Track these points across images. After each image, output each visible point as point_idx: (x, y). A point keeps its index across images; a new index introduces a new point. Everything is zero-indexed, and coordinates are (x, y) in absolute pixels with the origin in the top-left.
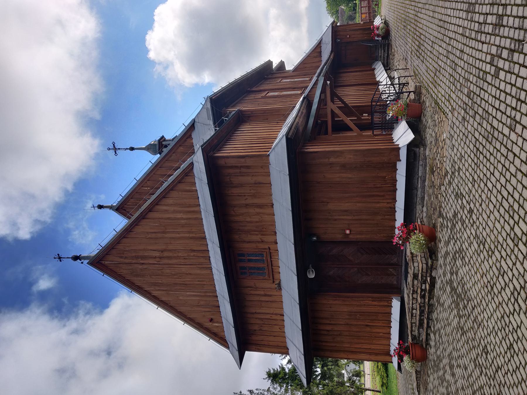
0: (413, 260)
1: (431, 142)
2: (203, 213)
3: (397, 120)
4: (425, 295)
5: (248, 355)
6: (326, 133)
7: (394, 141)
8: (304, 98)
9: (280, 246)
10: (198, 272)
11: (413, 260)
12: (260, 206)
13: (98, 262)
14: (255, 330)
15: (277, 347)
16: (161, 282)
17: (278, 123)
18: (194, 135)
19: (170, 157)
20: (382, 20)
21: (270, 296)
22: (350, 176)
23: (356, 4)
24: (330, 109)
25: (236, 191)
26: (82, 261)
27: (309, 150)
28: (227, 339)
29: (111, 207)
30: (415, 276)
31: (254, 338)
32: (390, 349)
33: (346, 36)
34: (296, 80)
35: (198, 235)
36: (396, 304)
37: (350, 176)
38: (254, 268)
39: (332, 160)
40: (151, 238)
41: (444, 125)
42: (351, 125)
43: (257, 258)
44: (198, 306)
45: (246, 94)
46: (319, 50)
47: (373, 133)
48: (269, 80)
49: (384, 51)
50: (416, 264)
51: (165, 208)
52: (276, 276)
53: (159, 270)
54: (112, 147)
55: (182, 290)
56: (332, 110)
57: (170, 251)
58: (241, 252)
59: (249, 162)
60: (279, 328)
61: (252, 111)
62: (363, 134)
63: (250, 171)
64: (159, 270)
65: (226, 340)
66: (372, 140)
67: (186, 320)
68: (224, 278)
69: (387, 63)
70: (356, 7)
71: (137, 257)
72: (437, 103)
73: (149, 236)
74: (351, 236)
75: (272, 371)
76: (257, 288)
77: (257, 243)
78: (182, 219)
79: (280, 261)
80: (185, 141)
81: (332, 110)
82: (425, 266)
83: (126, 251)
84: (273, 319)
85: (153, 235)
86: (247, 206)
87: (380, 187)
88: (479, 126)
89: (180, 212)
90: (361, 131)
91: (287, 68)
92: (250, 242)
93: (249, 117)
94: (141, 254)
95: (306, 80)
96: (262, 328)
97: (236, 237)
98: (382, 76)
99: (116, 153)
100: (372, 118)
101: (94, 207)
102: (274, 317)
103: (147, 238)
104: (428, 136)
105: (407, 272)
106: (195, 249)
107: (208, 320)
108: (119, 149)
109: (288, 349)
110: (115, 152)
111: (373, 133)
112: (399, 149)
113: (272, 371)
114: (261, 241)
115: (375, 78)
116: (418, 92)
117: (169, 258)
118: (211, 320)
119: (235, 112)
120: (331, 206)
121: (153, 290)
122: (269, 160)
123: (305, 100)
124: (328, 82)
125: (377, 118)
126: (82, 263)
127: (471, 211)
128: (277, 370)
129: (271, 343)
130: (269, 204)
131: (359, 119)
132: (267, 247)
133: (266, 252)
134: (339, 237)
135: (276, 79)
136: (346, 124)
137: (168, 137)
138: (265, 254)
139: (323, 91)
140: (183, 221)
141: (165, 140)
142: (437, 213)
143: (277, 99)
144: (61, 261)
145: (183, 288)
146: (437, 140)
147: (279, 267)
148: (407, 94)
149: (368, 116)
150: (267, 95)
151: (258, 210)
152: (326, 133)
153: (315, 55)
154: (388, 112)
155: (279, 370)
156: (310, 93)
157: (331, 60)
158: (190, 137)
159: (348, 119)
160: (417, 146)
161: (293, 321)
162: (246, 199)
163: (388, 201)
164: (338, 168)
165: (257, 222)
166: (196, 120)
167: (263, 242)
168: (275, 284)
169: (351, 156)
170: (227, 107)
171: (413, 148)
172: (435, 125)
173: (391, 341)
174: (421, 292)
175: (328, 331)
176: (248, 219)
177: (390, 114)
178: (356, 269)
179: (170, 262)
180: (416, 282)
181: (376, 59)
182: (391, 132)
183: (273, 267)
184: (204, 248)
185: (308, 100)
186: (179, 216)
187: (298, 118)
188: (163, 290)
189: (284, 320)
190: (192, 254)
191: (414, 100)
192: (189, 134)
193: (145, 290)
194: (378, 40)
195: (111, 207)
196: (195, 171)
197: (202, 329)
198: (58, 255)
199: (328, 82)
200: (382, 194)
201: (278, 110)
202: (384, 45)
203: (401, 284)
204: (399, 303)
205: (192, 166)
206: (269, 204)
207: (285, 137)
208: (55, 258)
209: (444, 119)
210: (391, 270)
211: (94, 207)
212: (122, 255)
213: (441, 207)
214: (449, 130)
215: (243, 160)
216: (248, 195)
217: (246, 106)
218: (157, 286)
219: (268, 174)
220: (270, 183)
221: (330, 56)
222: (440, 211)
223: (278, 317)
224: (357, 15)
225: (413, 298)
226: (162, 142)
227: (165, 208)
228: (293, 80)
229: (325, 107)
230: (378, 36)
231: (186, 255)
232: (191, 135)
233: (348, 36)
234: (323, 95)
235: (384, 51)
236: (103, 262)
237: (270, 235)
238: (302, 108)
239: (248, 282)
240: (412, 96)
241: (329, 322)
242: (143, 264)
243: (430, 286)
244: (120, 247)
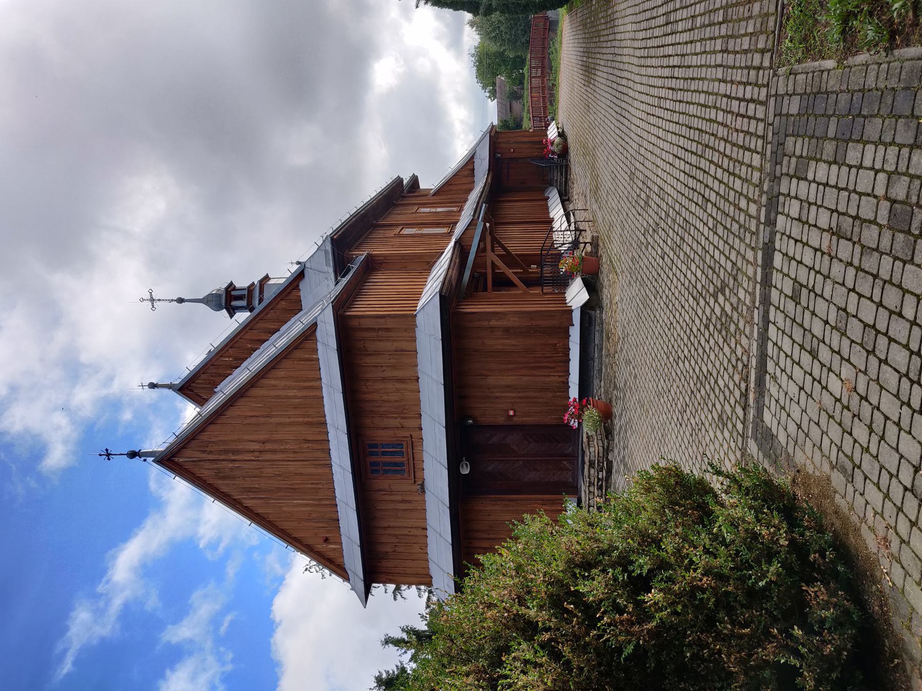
0: (589, 444)
2: (324, 390)
4: (602, 485)
5: (378, 590)
6: (485, 290)
8: (456, 243)
9: (426, 434)
10: (312, 470)
11: (589, 444)
12: (402, 380)
13: (169, 459)
14: (387, 552)
15: (417, 575)
16: (257, 486)
18: (303, 285)
19: (266, 314)
20: (558, 128)
21: (409, 502)
22: (513, 342)
23: (523, 74)
25: (370, 360)
27: (465, 310)
28: (347, 567)
29: (170, 387)
30: (592, 464)
31: (385, 564)
33: (509, 150)
34: (439, 210)
35: (315, 420)
37: (513, 342)
38: (390, 464)
39: (493, 323)
40: (250, 424)
44: (309, 520)
45: (371, 229)
46: (471, 167)
48: (401, 208)
49: (562, 174)
50: (592, 449)
51: (273, 382)
52: (418, 474)
53: (256, 469)
55: (288, 498)
57: (275, 441)
58: (374, 442)
59: (390, 324)
61: (386, 256)
63: (391, 334)
64: (256, 469)
65: (345, 569)
67: (291, 540)
68: (349, 477)
69: (565, 190)
70: (524, 79)
71: (227, 452)
72: (611, 261)
73: (248, 421)
74: (515, 419)
75: (384, 676)
76: (391, 493)
78: (296, 397)
80: (290, 293)
81: (492, 262)
82: (601, 449)
83: (213, 442)
84: (412, 536)
85: (253, 420)
86: (384, 379)
87: (550, 357)
89: (290, 388)
91: (423, 185)
92: (386, 428)
93: (381, 263)
94: (233, 447)
95: (453, 212)
96: (396, 548)
97: (368, 421)
98: (557, 212)
99: (153, 306)
100: (542, 271)
102: (414, 532)
103: (245, 425)
104: (604, 297)
105: (583, 463)
106: (310, 438)
107: (321, 541)
108: (159, 300)
110: (153, 304)
112: (572, 311)
113: (384, 676)
115: (548, 213)
116: (595, 243)
117: (274, 451)
118: (326, 540)
120: (491, 381)
121: (244, 499)
122: (415, 321)
123: (457, 246)
124: (488, 225)
125: (547, 270)
126: (145, 460)
127: (636, 377)
128: (394, 672)
129: (408, 571)
131: (526, 271)
132: (407, 434)
134: (501, 420)
135: (410, 207)
137: (238, 285)
138: (404, 444)
139: (482, 239)
140: (297, 401)
141: (235, 289)
142: (612, 386)
143: (416, 239)
144: (109, 459)
145: (288, 494)
146: (611, 302)
148: (583, 245)
151: (399, 385)
152: (485, 290)
153: (466, 173)
154: (560, 266)
155: (396, 673)
158: (297, 287)
160: (593, 309)
161: (440, 535)
163: (560, 374)
164: (500, 333)
165: (396, 401)
169: (516, 319)
170: (350, 249)
172: (610, 286)
174: (598, 482)
176: (385, 397)
177: (563, 269)
178: (521, 463)
179: (274, 457)
180: (592, 471)
181: (551, 184)
184: (324, 438)
185: (460, 244)
186: (291, 393)
187: (451, 270)
188: (263, 498)
190: (306, 446)
191: (591, 252)
192: (295, 284)
194: (553, 158)
195: (170, 387)
196: (319, 333)
197: (312, 554)
198: (107, 450)
200: (552, 365)
201: (420, 256)
202: (561, 166)
203: (577, 482)
207: (438, 295)
208: (100, 455)
210: (565, 463)
212: (206, 449)
213: (615, 377)
215: (383, 321)
217: (377, 247)
218: (253, 492)
219: (414, 340)
220: (416, 351)
222: (615, 382)
223: (420, 532)
224: (526, 92)
225: (590, 492)
226: (230, 291)
227: (273, 382)
228: (433, 210)
229: (483, 254)
230: (553, 153)
231: (296, 447)
232: (298, 286)
233: (512, 150)
235: (562, 174)
236: (176, 459)
237: (413, 418)
238: (454, 256)
239: (382, 483)
240: (589, 248)
241: (487, 536)
242: (234, 460)
243: (607, 473)
244: (204, 437)
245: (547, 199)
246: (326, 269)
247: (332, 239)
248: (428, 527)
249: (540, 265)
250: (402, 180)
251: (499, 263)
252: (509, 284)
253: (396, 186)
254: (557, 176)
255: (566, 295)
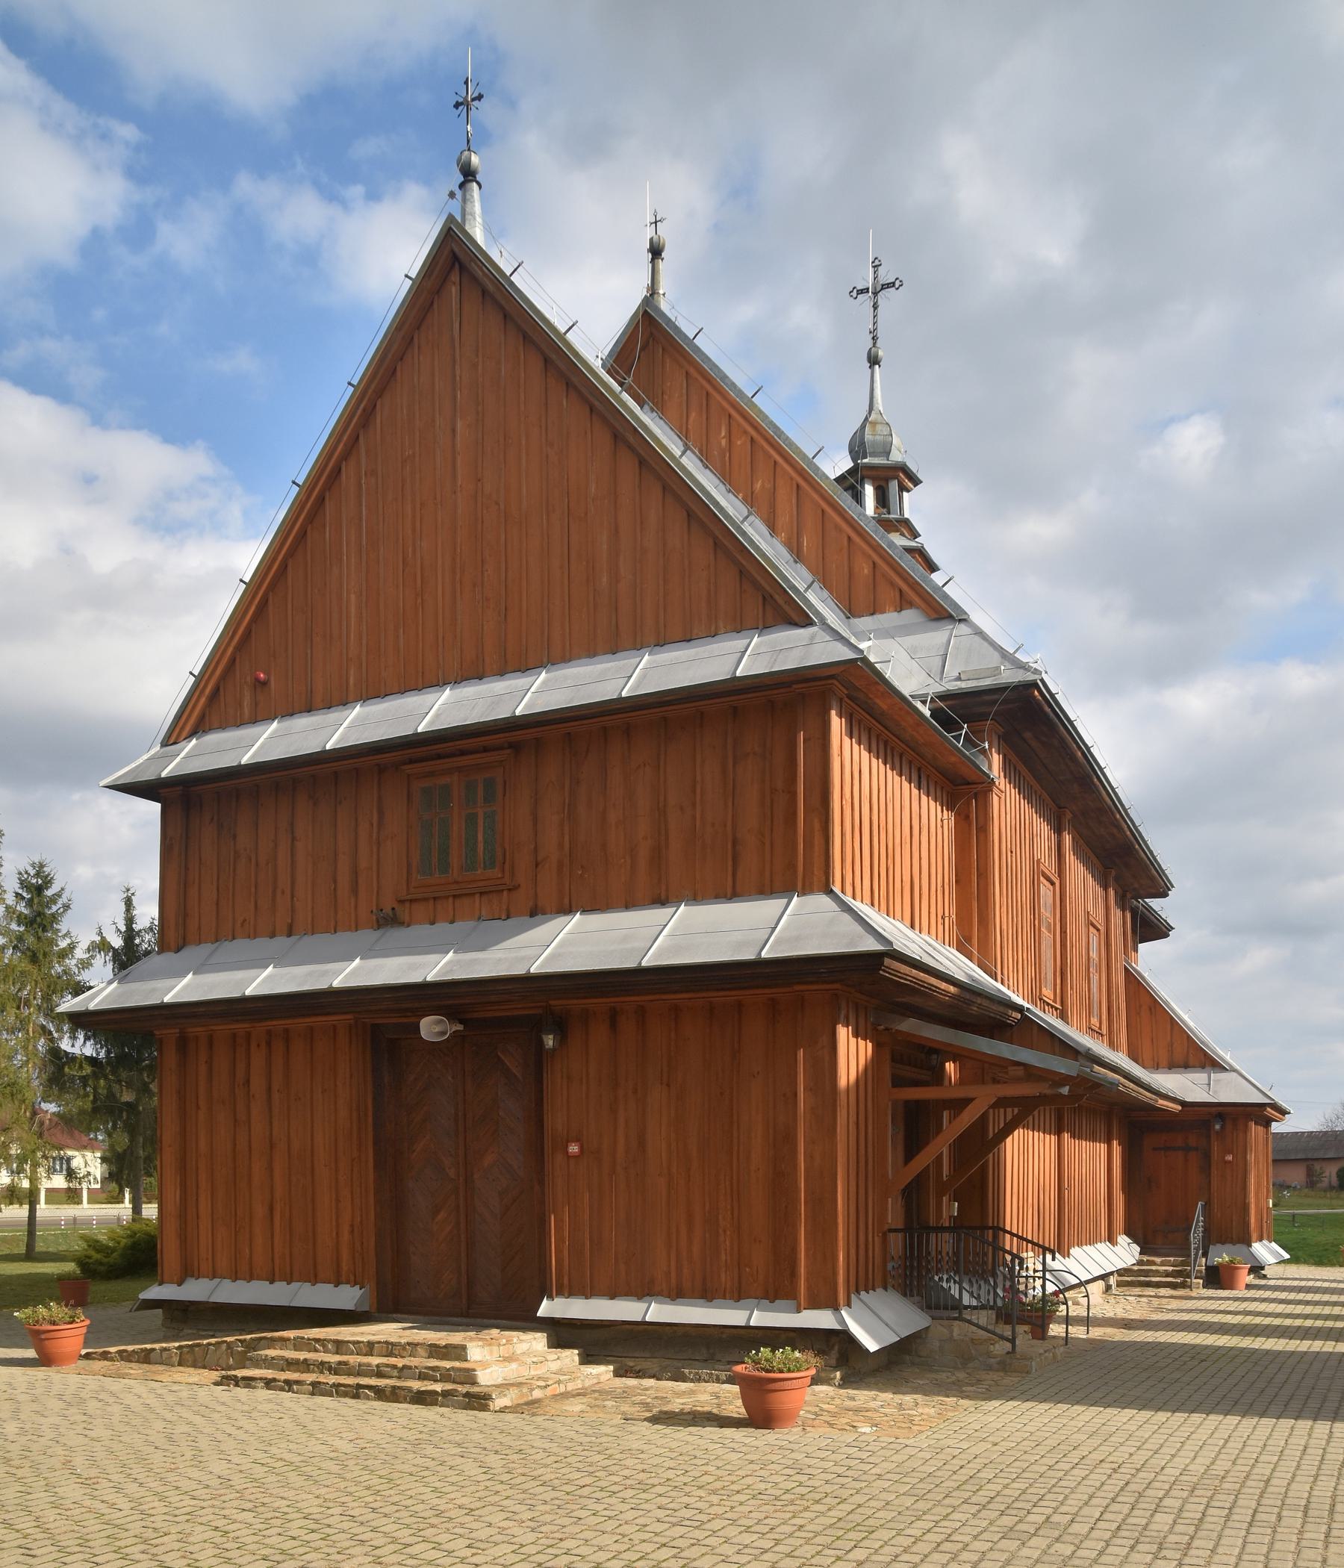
1: (853, 1399)
3: (929, 1307)
7: (863, 1293)
12: (658, 856)
14: (235, 837)
17: (943, 918)
24: (971, 1095)
26: (459, 194)
32: (204, 1277)
36: (346, 1297)
41: (899, 1427)
42: (923, 1160)
43: (481, 846)
47: (891, 1230)
49: (1167, 1274)
54: (885, 276)
56: (972, 1100)
60: (245, 920)
62: (890, 1200)
66: (870, 1227)
77: (532, 847)
79: (472, 924)
81: (972, 1100)
88: (883, 1503)
90: (904, 1191)
91: (1148, 951)
99: (861, 292)
101: (656, 222)
108: (875, 307)
109: (178, 950)
111: (891, 1230)
114: (539, 859)
115: (1080, 1244)
119: (985, 769)
124: (1065, 1090)
130: (667, 890)
133: (500, 876)
134: (556, 1121)
136: (928, 1144)
137: (912, 505)
139: (1031, 1073)
141: (903, 488)
144: (457, 105)
147: (452, 922)
148: (1008, 1334)
149: (950, 1217)
150: (1042, 878)
152: (898, 1082)
156: (1035, 1028)
157: (1152, 1102)
158: (903, 603)
159: (945, 1151)
162: (682, 809)
166: (962, 629)
167: (537, 866)
168: (395, 905)
171: (836, 1348)
173: (227, 1282)
175: (248, 1082)
182: (893, 1287)
183: (451, 900)
189: (273, 935)
193: (361, 438)
198: (480, 97)
199: (1067, 1088)
204: (349, 1305)
205: (796, 619)
206: (667, 890)
209: (915, 1428)
211: (656, 222)
214: (881, 1439)
216: (694, 817)
221: (1174, 1100)
226: (897, 477)
232: (911, 605)
233: (1229, 1158)
234: (1020, 1072)
235: (1167, 1274)
236: (455, 277)
238: (986, 1003)
245: (1111, 1239)
246: (951, 671)
247: (1034, 685)
248: (294, 938)
249: (957, 1227)
250: (1164, 895)
251: (968, 1117)
252: (912, 1145)
253: (1152, 879)
254: (1162, 1264)
255: (880, 1291)
